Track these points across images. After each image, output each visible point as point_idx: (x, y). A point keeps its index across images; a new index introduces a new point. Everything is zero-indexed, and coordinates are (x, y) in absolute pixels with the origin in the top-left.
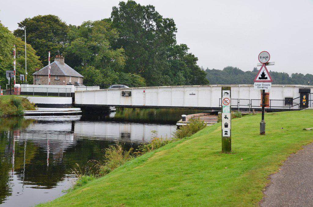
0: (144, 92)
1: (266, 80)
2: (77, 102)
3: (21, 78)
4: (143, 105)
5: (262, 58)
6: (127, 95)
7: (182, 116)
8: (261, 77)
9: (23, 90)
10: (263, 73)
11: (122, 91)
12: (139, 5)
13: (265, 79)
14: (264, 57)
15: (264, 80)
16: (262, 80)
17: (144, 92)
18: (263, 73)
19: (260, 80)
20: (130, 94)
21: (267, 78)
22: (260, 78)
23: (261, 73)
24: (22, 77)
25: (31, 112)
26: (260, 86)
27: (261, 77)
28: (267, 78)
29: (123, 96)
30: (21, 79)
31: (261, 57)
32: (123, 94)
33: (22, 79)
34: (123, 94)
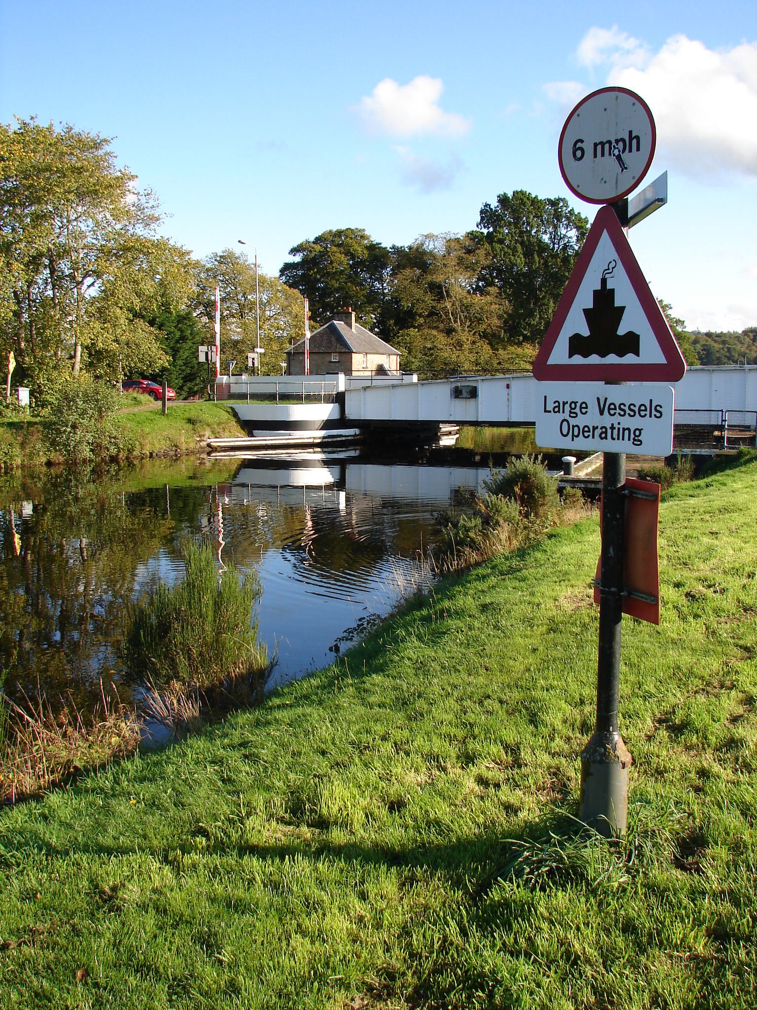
0: (508, 386)
1: (630, 359)
2: (352, 413)
3: (250, 360)
4: (506, 420)
5: (589, 151)
6: (465, 394)
7: (563, 459)
8: (585, 332)
9: (234, 389)
10: (604, 296)
11: (454, 385)
12: (536, 197)
13: (621, 354)
14: (600, 147)
15: (612, 359)
16: (594, 359)
17: (508, 386)
18: (604, 296)
19: (578, 360)
20: (473, 393)
21: (631, 343)
22: (577, 345)
23: (584, 299)
24: (253, 359)
25: (229, 442)
26: (581, 421)
27: (585, 332)
28: (631, 343)
29: (457, 397)
30: (250, 364)
31: (578, 151)
32: (457, 393)
33: (253, 363)
34: (457, 393)
